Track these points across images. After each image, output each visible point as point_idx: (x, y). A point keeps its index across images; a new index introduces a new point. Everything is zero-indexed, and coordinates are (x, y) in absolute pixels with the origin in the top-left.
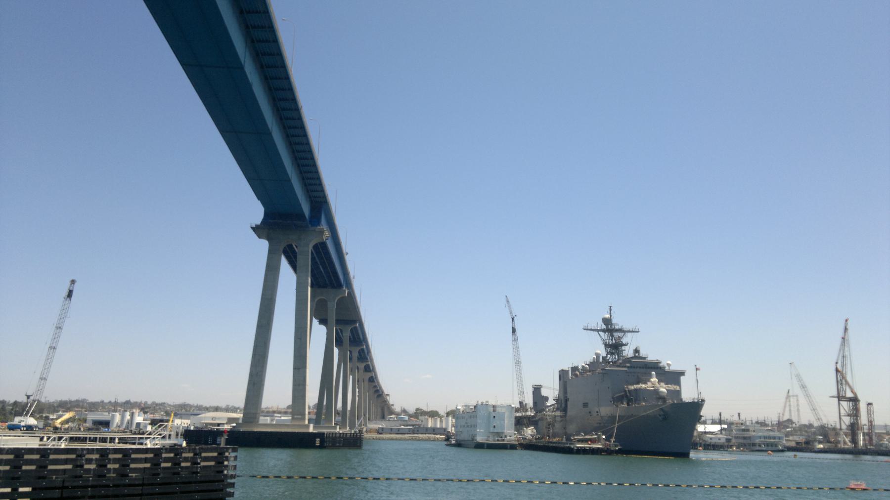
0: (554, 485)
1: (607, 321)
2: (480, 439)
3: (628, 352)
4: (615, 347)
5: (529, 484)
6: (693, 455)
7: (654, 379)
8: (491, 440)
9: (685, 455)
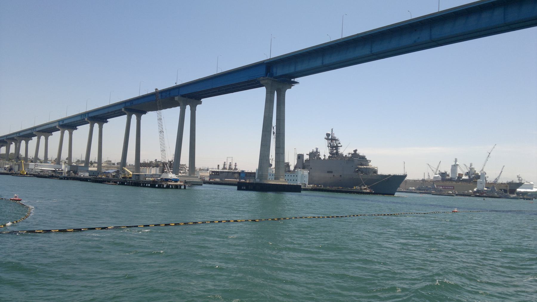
1: (328, 135)
3: (345, 151)
6: (397, 194)
9: (393, 194)
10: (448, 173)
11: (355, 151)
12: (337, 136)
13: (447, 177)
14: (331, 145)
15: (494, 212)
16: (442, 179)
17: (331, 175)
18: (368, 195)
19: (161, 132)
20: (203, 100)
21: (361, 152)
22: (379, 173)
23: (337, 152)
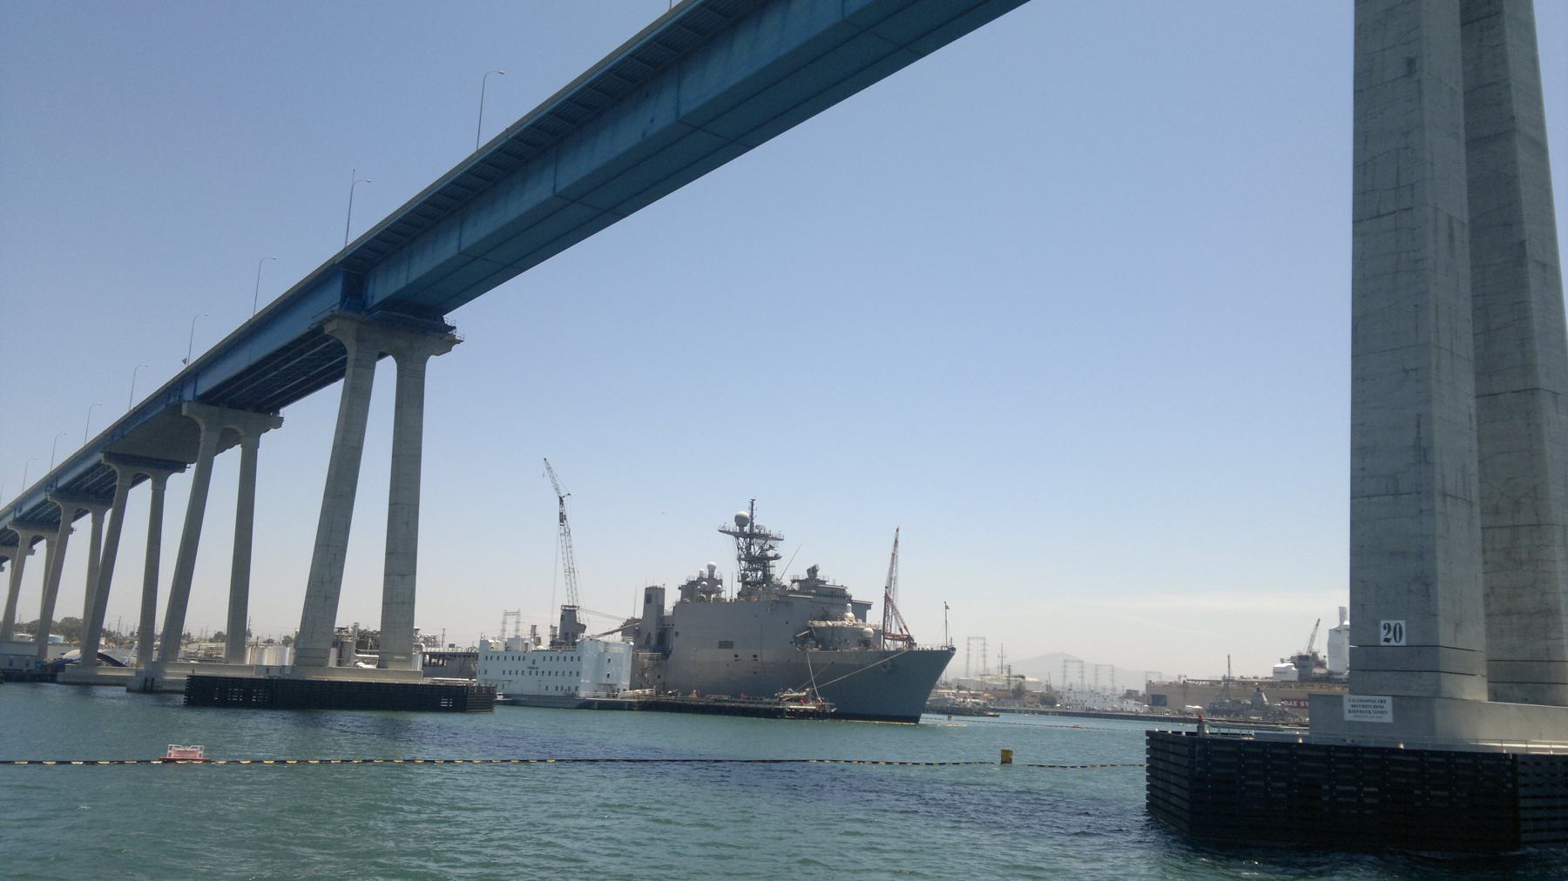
0: (89, 768)
1: (741, 521)
2: (584, 694)
3: (787, 571)
4: (757, 561)
5: (35, 769)
6: (926, 719)
7: (850, 614)
8: (603, 696)
9: (916, 719)
10: (1320, 656)
11: (813, 571)
12: (763, 521)
13: (1318, 671)
14: (749, 553)
15: (584, 767)
16: (1300, 676)
17: (726, 655)
18: (704, 717)
19: (570, 571)
20: (283, 412)
21: (831, 576)
22: (639, 615)
23: (767, 578)
